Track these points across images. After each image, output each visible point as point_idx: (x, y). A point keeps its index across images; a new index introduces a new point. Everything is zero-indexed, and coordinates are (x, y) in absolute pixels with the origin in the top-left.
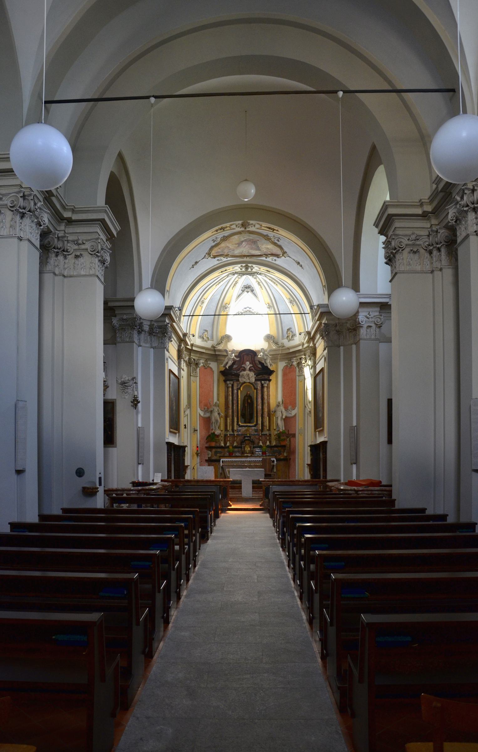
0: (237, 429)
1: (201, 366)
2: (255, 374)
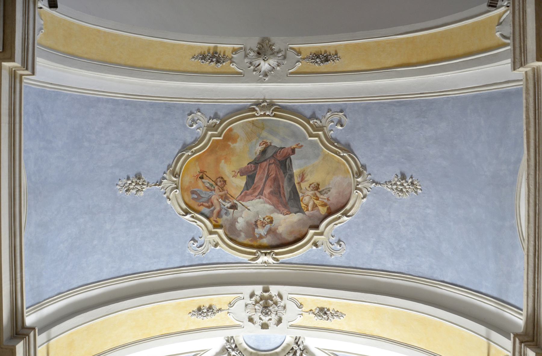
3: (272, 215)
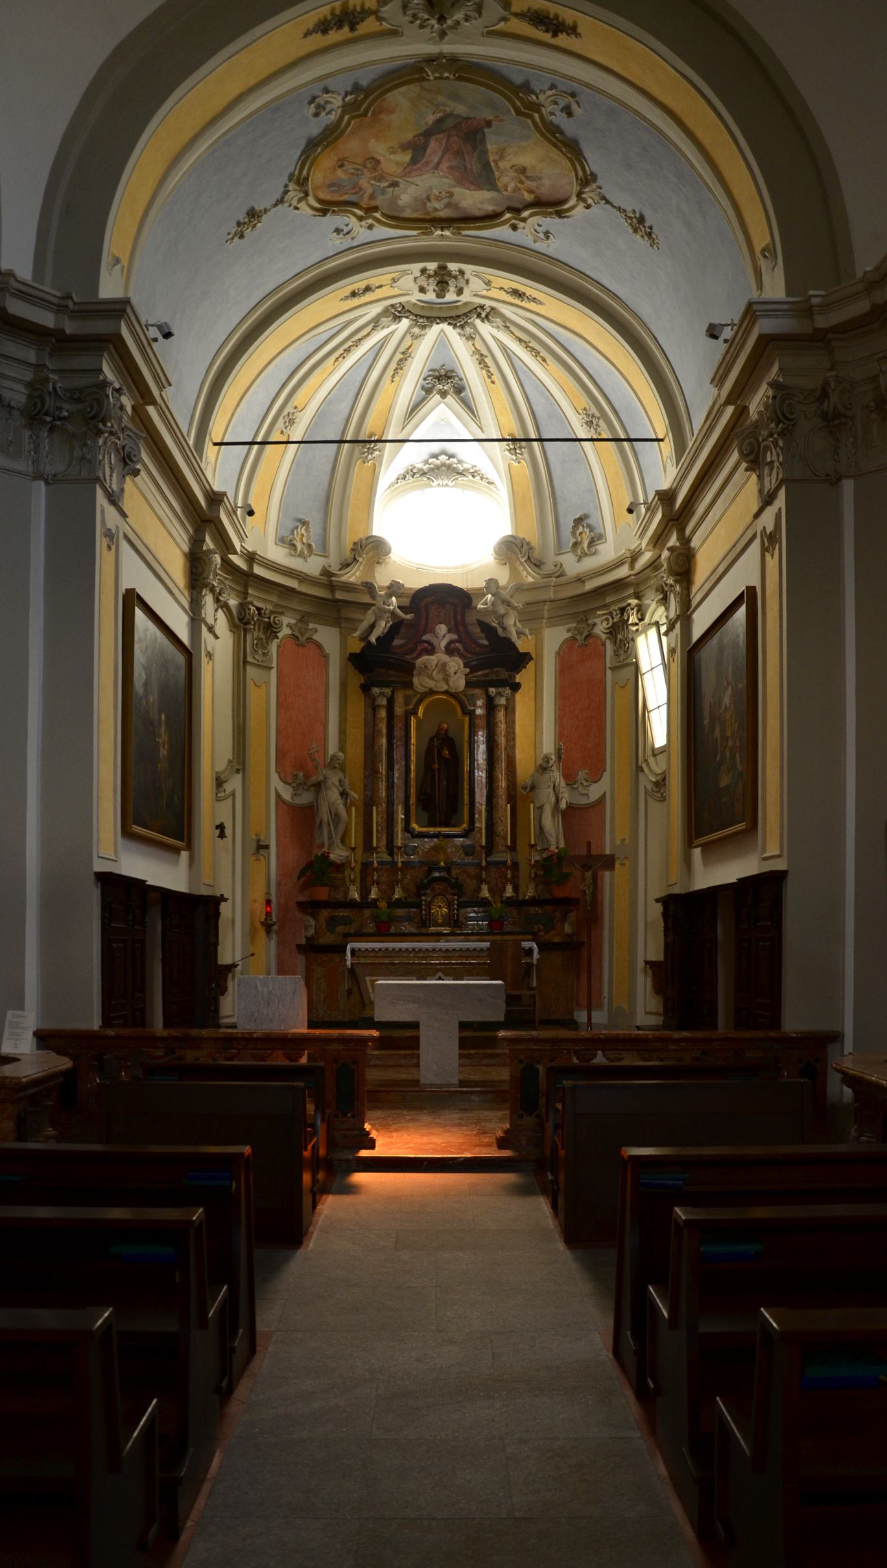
0: (406, 846)
1: (285, 637)
2: (465, 665)
3: (451, 190)
